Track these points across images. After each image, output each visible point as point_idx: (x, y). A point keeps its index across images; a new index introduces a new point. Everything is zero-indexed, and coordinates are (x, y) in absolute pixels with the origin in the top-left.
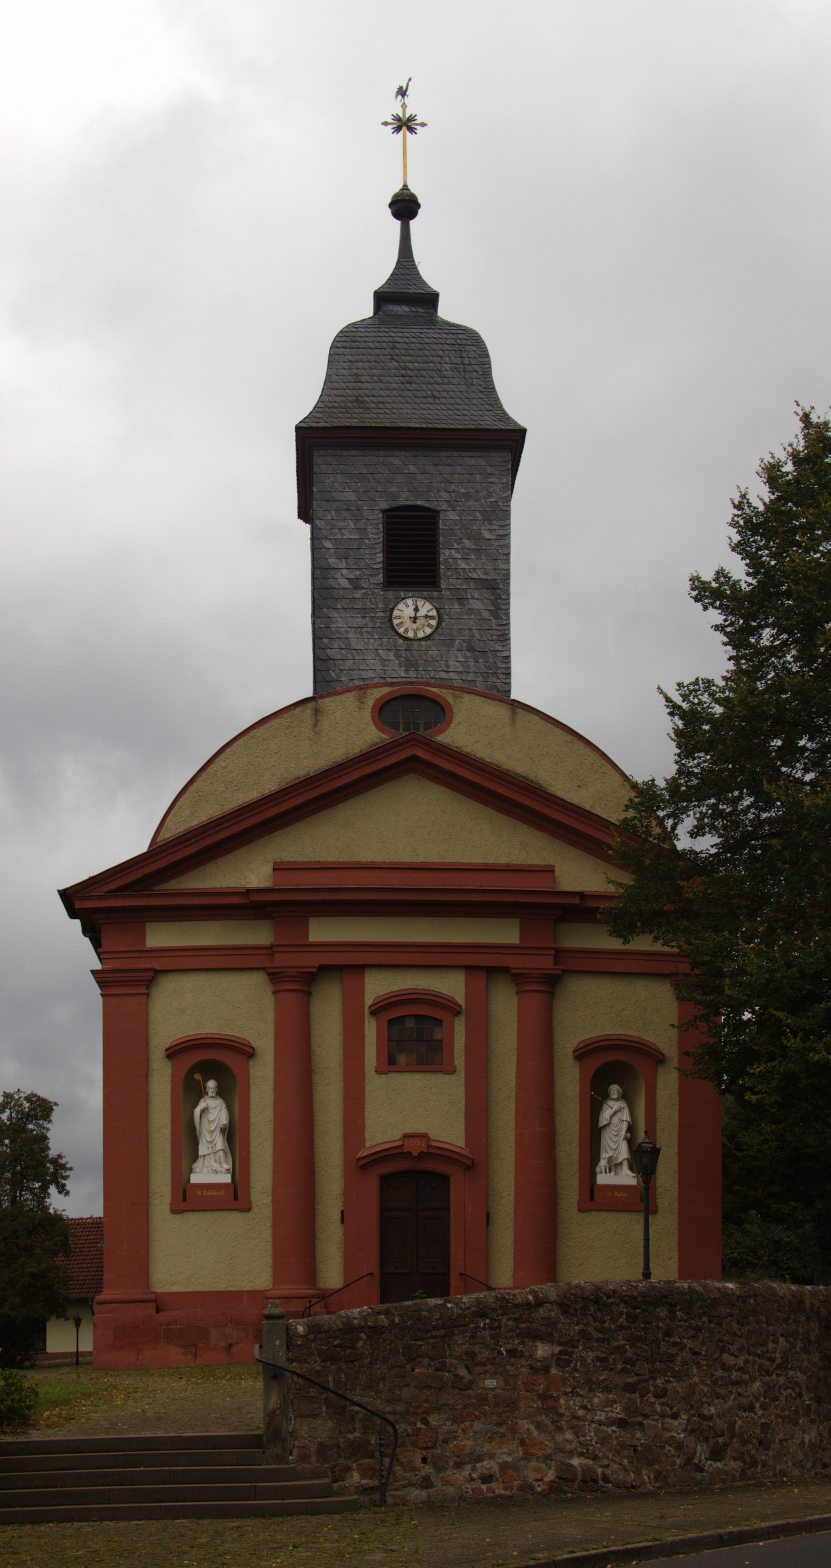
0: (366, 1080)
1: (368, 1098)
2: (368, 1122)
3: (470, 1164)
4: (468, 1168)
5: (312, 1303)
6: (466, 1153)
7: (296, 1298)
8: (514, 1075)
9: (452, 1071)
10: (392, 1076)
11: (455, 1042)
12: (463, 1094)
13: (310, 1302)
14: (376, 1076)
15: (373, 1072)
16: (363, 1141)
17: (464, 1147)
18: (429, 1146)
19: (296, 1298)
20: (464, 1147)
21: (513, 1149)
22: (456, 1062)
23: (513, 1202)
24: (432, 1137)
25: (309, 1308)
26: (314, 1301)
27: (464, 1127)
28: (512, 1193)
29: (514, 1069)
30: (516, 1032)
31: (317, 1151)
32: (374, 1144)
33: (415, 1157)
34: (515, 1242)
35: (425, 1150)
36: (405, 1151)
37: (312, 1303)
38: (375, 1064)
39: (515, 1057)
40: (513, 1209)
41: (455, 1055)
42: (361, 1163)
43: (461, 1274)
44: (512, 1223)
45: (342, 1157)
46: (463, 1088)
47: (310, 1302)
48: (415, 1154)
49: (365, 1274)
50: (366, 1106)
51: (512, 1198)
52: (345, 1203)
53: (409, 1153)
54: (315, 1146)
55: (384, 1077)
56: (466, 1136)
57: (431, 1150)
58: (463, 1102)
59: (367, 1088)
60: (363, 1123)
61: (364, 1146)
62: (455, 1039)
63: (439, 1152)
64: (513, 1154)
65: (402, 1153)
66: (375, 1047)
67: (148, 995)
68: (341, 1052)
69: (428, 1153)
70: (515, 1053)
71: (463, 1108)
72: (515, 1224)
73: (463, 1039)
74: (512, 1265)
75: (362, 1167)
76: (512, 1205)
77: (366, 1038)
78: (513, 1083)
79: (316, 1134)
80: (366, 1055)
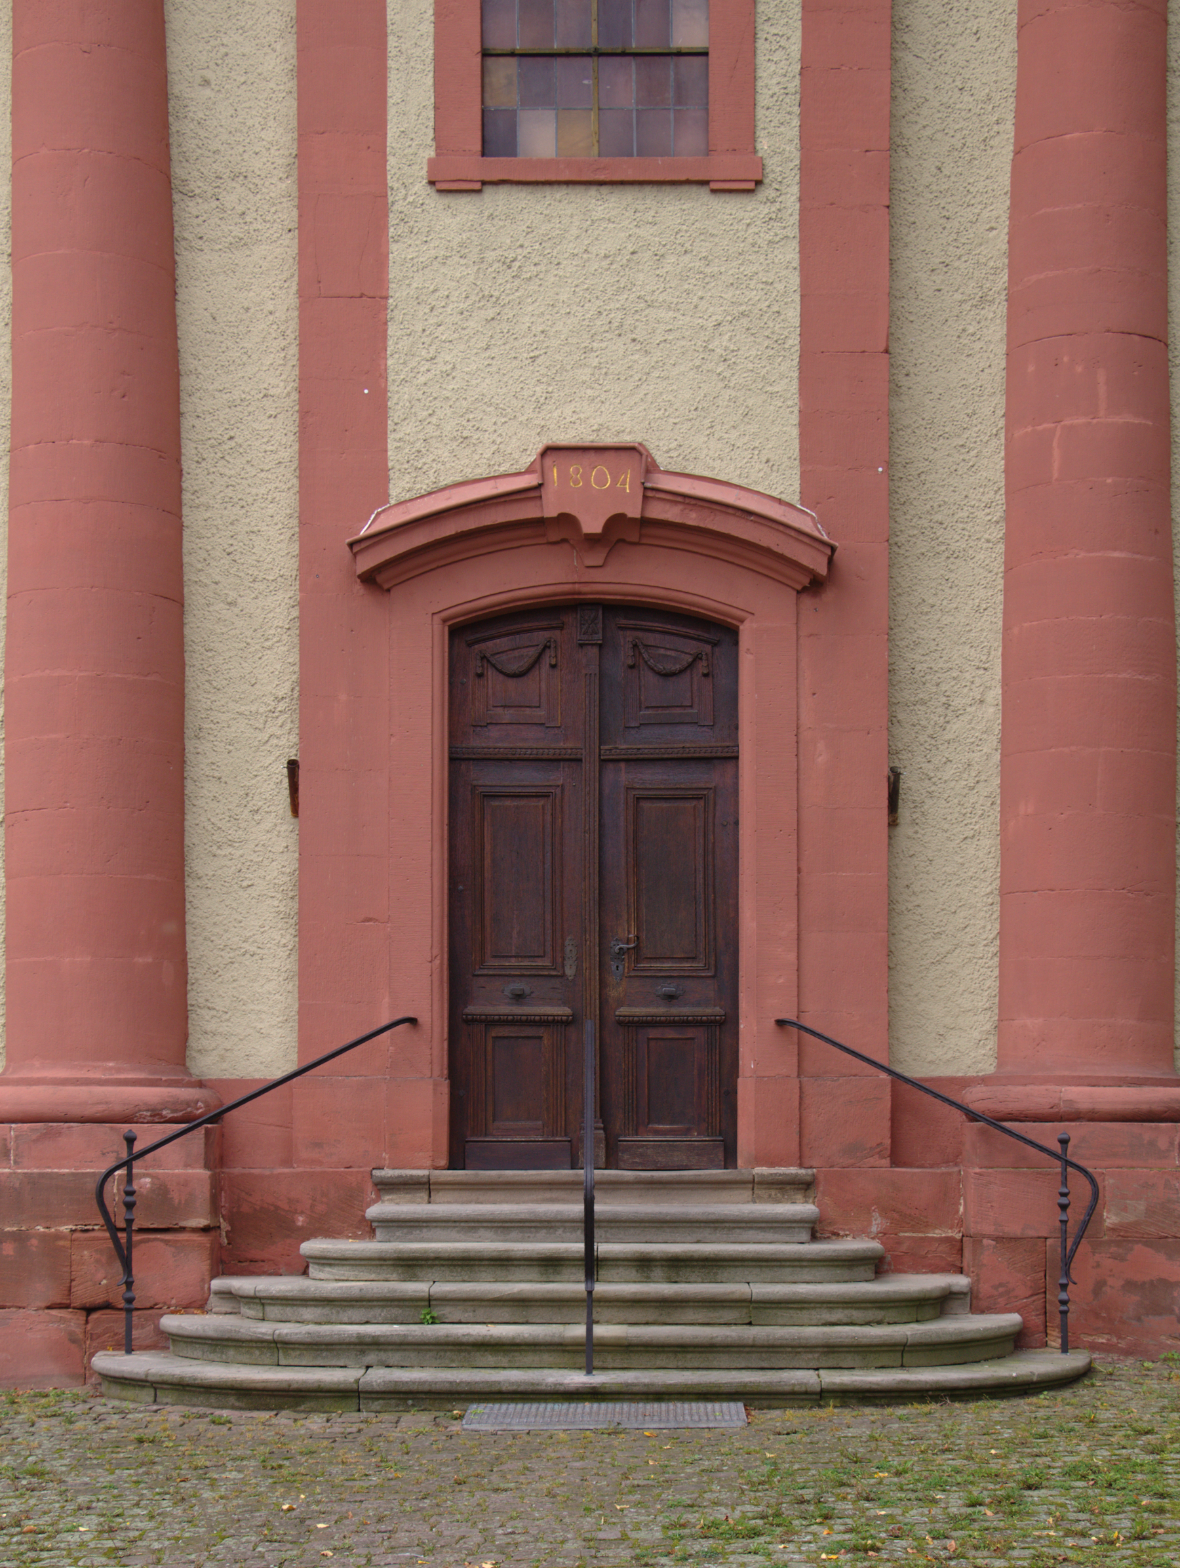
0: (393, 219)
1: (399, 294)
2: (399, 397)
3: (822, 570)
4: (815, 585)
5: (138, 1147)
6: (806, 525)
7: (83, 1120)
8: (1001, 207)
9: (752, 186)
10: (498, 200)
11: (761, 59)
12: (795, 280)
13: (130, 1140)
14: (435, 202)
15: (420, 187)
16: (380, 475)
17: (795, 500)
18: (649, 494)
19: (83, 1120)
20: (795, 500)
21: (999, 512)
22: (764, 145)
23: (997, 729)
24: (662, 460)
25: (128, 1164)
26: (147, 1135)
27: (795, 419)
28: (995, 694)
29: (1004, 180)
30: (1014, 20)
31: (190, 517)
32: (423, 487)
33: (593, 541)
34: (1005, 892)
35: (634, 512)
36: (551, 511)
37: (138, 1147)
38: (431, 153)
39: (1009, 128)
40: (997, 757)
41: (760, 113)
42: (367, 562)
43: (781, 1023)
44: (995, 814)
45: (295, 548)
46: (791, 254)
47: (130, 1140)
48: (592, 524)
49: (385, 1022)
50: (392, 330)
51: (991, 713)
52: (307, 731)
53: (567, 520)
54: (186, 497)
55: (465, 206)
56: (806, 456)
57: (659, 511)
58: (793, 314)
59: (397, 252)
60: (379, 404)
61: (386, 496)
62: (761, 46)
63: (692, 518)
64: (998, 532)
65: (540, 522)
66: (429, 81)
67: (540, 497)
68: (288, 107)
69: (645, 522)
70: (1007, 110)
71: (794, 341)
72: (1004, 823)
73: (795, 47)
74: (992, 983)
75: (369, 579)
76: (992, 743)
77: (392, 42)
78: (1000, 240)
79: (189, 450)
80: (392, 112)
